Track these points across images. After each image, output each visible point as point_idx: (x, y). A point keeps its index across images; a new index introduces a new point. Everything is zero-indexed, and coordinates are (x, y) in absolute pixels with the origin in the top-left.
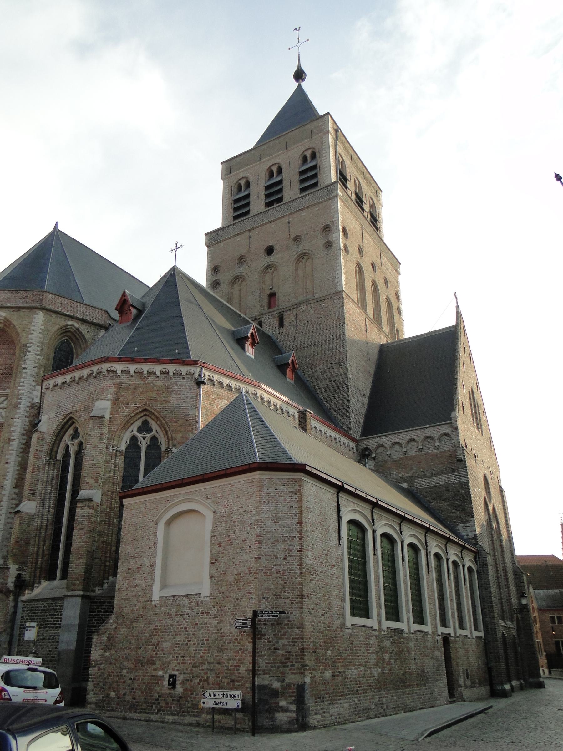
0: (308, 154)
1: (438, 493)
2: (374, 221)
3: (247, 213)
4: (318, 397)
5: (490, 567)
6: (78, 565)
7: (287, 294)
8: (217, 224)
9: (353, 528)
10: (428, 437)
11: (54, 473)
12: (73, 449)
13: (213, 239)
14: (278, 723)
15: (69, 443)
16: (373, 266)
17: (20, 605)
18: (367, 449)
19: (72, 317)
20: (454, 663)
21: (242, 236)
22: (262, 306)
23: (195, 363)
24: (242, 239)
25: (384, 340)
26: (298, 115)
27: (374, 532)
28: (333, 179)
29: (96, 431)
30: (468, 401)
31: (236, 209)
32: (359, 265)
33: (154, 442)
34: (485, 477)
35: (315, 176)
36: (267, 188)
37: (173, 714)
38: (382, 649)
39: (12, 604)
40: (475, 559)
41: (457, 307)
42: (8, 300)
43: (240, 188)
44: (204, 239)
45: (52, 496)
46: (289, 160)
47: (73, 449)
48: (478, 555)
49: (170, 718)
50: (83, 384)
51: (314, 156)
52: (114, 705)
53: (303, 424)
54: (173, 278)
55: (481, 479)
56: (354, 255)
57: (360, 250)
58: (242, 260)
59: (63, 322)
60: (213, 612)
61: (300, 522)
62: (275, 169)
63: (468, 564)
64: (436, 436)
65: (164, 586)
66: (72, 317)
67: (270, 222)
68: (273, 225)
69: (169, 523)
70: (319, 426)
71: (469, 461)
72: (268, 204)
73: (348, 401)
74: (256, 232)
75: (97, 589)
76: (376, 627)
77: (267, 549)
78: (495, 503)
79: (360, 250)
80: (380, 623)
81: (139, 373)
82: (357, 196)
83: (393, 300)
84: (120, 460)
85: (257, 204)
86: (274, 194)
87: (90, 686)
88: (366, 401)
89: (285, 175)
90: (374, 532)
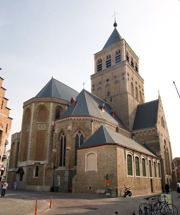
0: (118, 51)
1: (152, 145)
2: (137, 69)
3: (101, 69)
4: (122, 122)
5: (164, 163)
6: (67, 163)
7: (113, 92)
8: (93, 73)
9: (129, 157)
10: (149, 131)
11: (60, 143)
12: (63, 137)
13: (93, 77)
14: (112, 196)
15: (62, 136)
16: (136, 83)
17: (55, 172)
18: (133, 134)
19: (59, 103)
20: (153, 185)
21: (100, 76)
22: (106, 96)
23: (91, 116)
24: (100, 77)
25: (139, 103)
26: (115, 38)
27: (133, 157)
28: (125, 59)
29: (69, 134)
30: (161, 120)
31: (98, 68)
32: (132, 83)
33: (82, 136)
34: (165, 140)
35: (120, 58)
36: (107, 62)
37: (90, 194)
38: (135, 182)
39: (53, 172)
40: (160, 161)
41: (159, 94)
42: (44, 100)
43: (99, 62)
44: (90, 77)
45: (60, 148)
46: (113, 53)
47: (63, 137)
48: (161, 160)
49: (90, 195)
50: (64, 122)
51: (119, 52)
52: (78, 192)
53: (117, 130)
54: (84, 91)
55: (163, 141)
56: (131, 81)
57: (132, 79)
58: (100, 83)
59: (57, 105)
60: (98, 174)
61: (116, 156)
62: (109, 56)
63: (158, 162)
64: (151, 130)
65: (87, 169)
66: (59, 103)
67: (108, 72)
68: (108, 73)
69: (87, 155)
70: (121, 129)
71: (160, 137)
72: (107, 67)
73: (129, 121)
74: (104, 75)
75: (72, 168)
76: (134, 177)
77: (109, 162)
78: (167, 146)
79: (132, 79)
80: (135, 176)
81: (77, 119)
82: (132, 62)
83: (142, 92)
84: (74, 140)
85: (104, 67)
86: (108, 64)
87: (73, 188)
88: (134, 121)
89: (111, 58)
90: (133, 157)
